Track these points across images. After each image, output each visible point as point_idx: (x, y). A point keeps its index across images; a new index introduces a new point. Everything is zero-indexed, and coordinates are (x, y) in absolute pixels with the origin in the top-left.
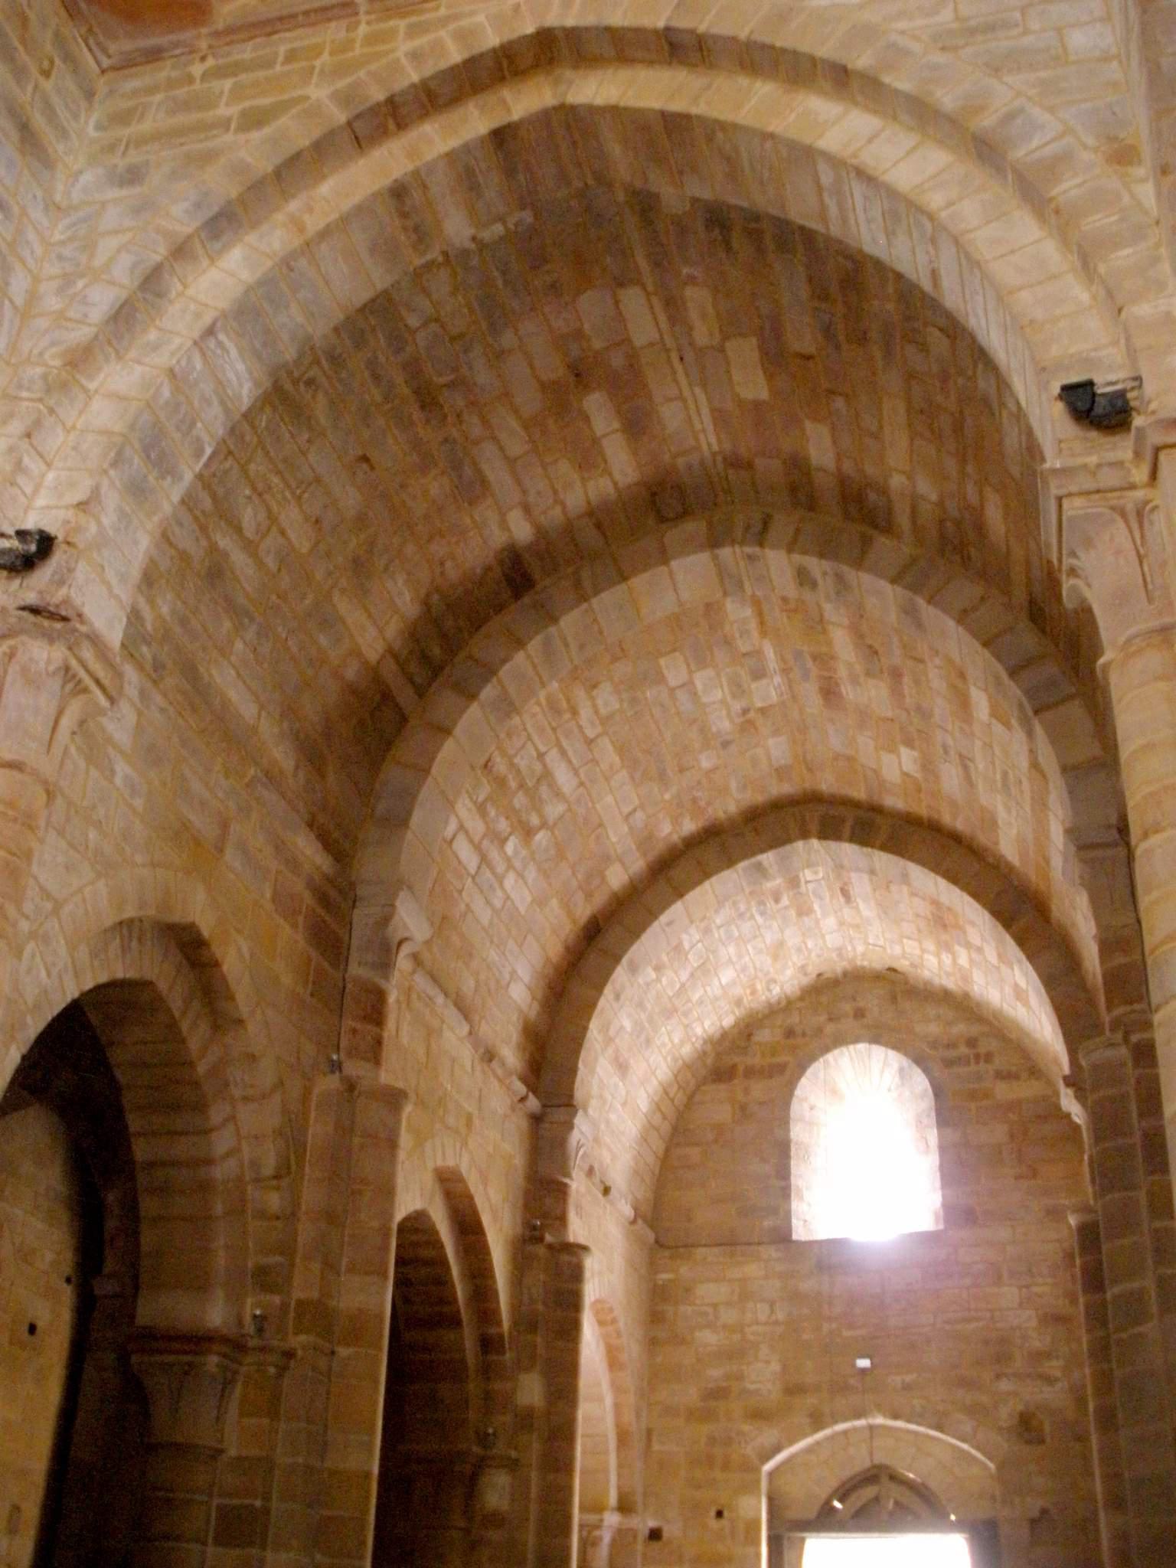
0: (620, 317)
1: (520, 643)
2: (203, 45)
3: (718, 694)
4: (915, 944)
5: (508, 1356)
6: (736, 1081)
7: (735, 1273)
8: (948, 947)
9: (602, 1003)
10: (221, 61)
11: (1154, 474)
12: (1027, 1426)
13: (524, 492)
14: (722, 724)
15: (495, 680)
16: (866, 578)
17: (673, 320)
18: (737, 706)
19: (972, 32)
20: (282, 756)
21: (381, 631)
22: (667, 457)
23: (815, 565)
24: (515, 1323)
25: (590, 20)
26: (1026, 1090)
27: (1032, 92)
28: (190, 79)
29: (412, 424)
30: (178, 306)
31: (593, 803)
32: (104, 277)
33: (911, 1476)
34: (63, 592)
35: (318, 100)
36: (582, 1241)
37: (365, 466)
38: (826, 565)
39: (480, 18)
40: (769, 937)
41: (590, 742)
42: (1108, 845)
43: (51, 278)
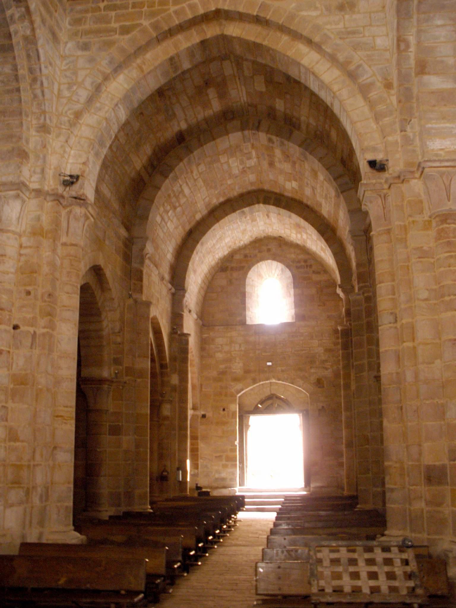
1: (181, 160)
4: (289, 231)
5: (169, 369)
6: (228, 272)
7: (229, 335)
8: (300, 233)
9: (193, 256)
10: (110, 3)
11: (389, 187)
12: (319, 383)
14: (236, 171)
15: (173, 172)
16: (291, 144)
18: (241, 167)
19: (349, 33)
20: (116, 205)
21: (142, 161)
22: (230, 104)
23: (274, 138)
24: (170, 359)
25: (232, 8)
26: (322, 277)
27: (365, 59)
28: (99, 9)
31: (194, 196)
32: (83, 86)
33: (282, 397)
34: (82, 191)
35: (145, 26)
36: (188, 333)
37: (142, 115)
38: (278, 138)
40: (242, 228)
41: (195, 180)
42: (360, 236)
43: (64, 84)
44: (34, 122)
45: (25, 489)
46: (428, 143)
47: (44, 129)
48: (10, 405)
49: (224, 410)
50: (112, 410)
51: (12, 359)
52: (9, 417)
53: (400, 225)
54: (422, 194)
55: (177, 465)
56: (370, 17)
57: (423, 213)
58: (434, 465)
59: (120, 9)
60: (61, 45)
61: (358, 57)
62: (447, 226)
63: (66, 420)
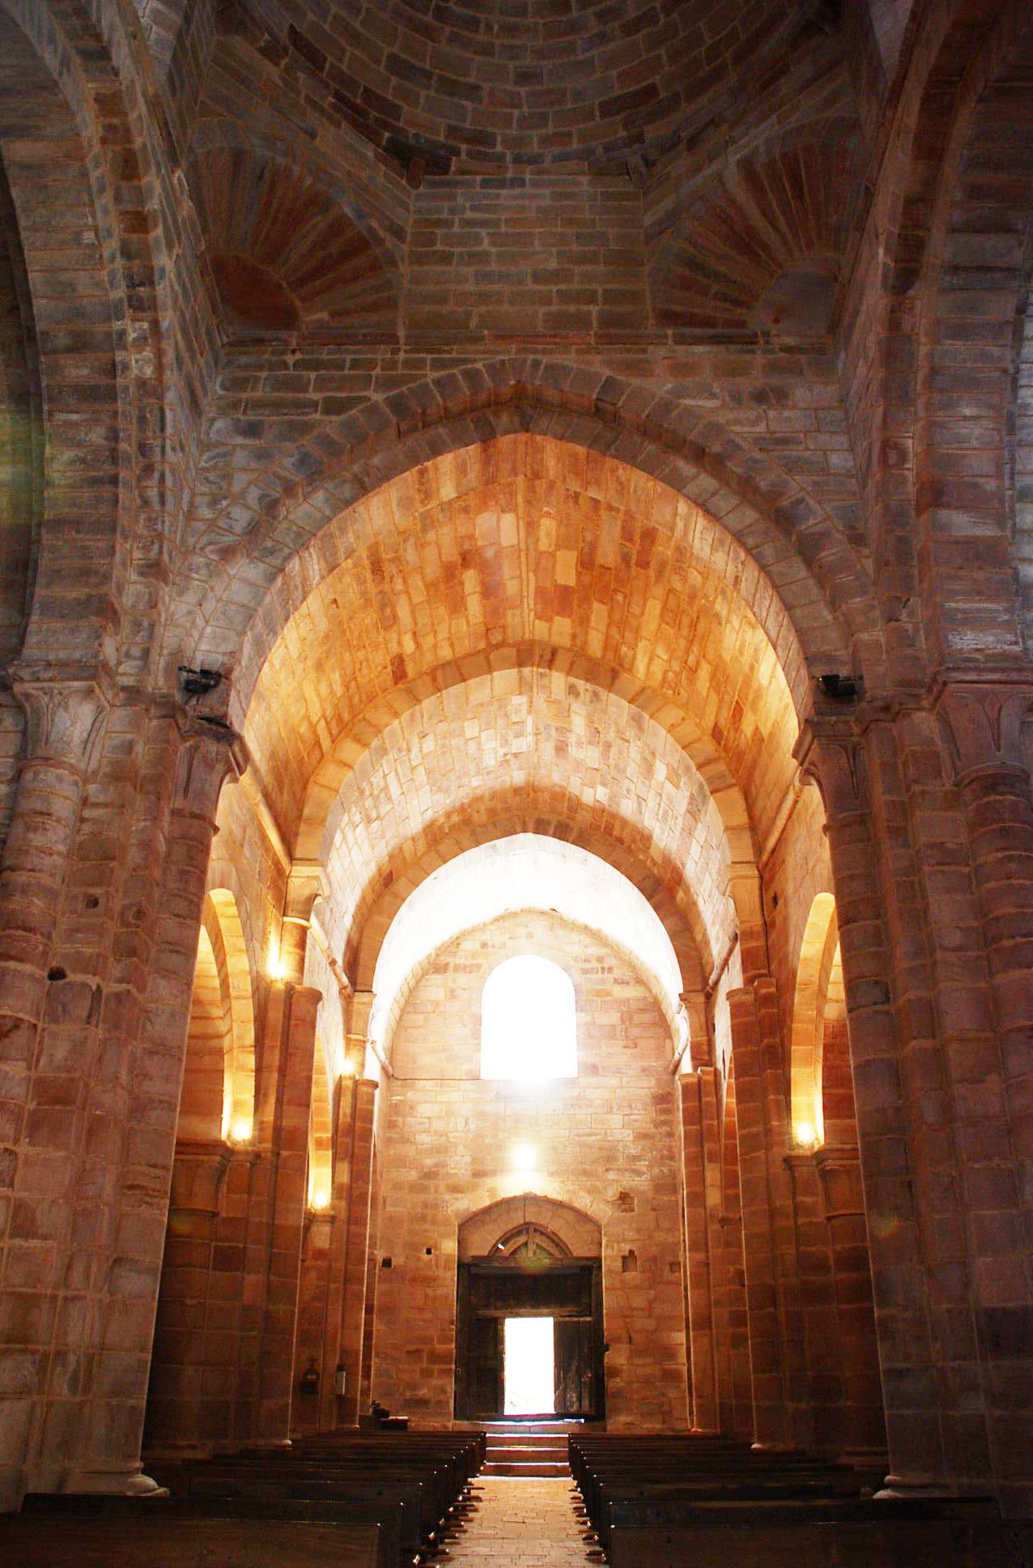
0: (498, 528)
2: (294, 342)
3: (493, 744)
10: (306, 357)
13: (416, 624)
16: (613, 697)
17: (528, 534)
18: (501, 752)
19: (777, 442)
23: (581, 684)
29: (365, 582)
30: (285, 525)
38: (589, 686)
39: (479, 365)
41: (413, 769)
44: (137, 554)
45: (38, 1357)
46: (950, 637)
47: (155, 569)
48: (24, 1148)
49: (429, 1252)
50: (224, 1215)
51: (41, 1043)
52: (17, 1180)
53: (893, 802)
54: (937, 739)
55: (336, 1360)
56: (816, 418)
57: (941, 778)
58: (1004, 1309)
59: (326, 368)
60: (204, 420)
61: (797, 485)
62: (998, 797)
63: (150, 1196)
